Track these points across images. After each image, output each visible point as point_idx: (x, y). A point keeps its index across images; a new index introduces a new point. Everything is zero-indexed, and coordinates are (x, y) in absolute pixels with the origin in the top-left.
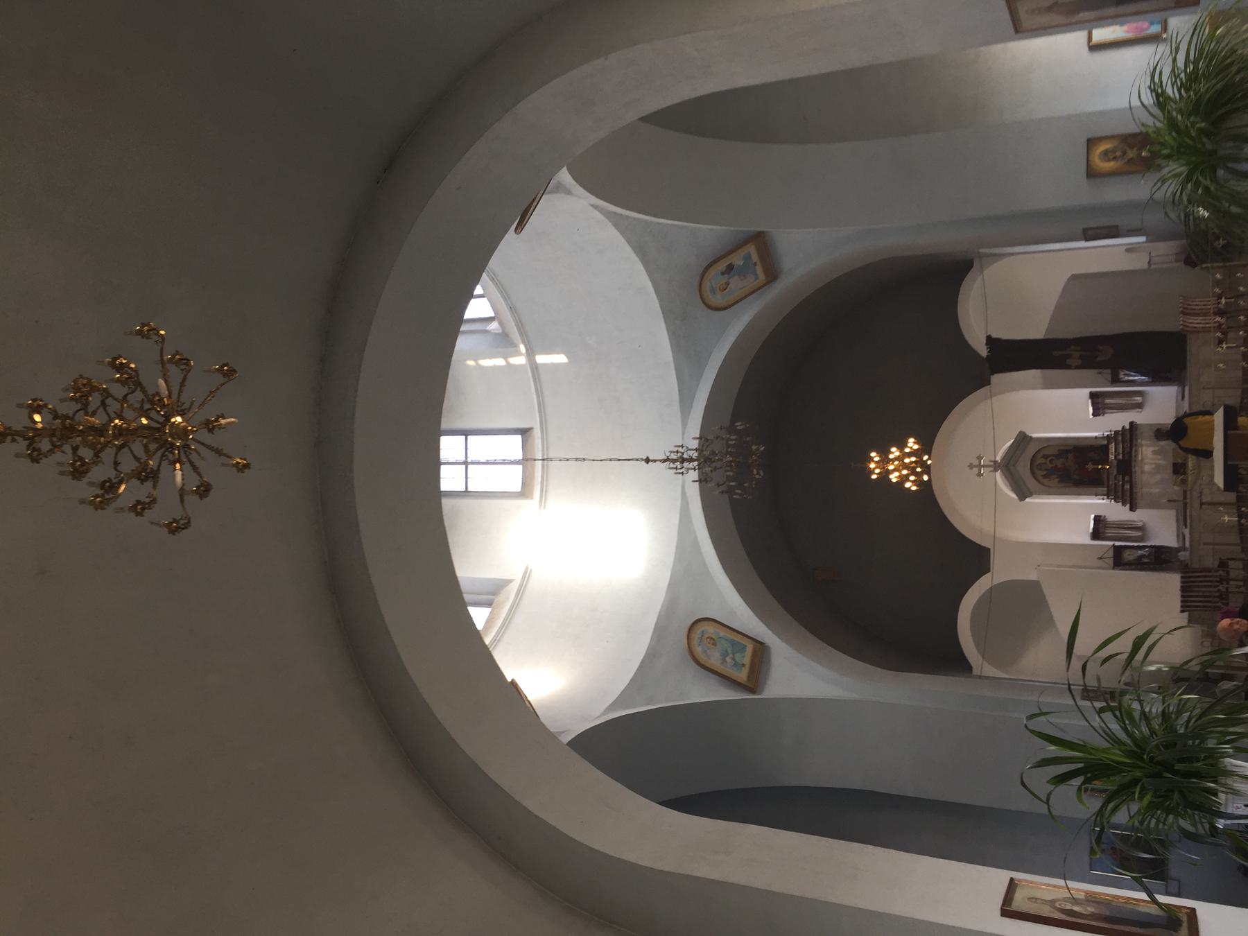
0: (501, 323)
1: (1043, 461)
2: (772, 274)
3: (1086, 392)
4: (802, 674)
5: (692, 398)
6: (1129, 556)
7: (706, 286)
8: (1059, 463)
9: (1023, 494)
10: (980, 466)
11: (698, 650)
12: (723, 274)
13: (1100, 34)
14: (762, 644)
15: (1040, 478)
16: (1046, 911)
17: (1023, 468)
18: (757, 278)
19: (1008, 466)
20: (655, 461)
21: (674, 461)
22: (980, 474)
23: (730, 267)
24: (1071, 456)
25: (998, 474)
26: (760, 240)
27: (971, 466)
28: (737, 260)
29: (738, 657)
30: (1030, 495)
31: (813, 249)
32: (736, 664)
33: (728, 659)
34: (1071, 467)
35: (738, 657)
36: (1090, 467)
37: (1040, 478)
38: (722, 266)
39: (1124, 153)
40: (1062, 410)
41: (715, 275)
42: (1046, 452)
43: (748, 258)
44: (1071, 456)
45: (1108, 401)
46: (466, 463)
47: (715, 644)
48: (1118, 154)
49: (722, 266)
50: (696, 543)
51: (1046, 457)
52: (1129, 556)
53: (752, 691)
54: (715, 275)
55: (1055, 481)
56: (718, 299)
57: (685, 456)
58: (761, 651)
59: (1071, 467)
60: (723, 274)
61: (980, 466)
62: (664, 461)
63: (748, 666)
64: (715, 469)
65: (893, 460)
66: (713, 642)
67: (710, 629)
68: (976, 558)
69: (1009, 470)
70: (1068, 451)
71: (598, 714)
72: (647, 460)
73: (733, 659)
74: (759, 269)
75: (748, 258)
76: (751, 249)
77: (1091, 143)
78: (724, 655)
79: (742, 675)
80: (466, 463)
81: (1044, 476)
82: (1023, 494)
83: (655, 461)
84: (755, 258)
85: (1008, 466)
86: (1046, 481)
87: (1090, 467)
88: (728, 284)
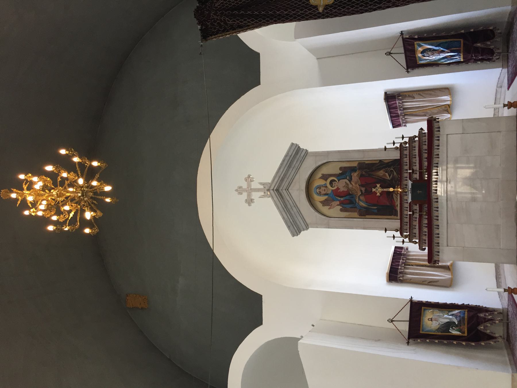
0: (419, 139)
1: (322, 182)
3: (379, 88)
6: (432, 322)
8: (341, 185)
9: (296, 227)
13: (445, 244)
16: (443, 90)
19: (279, 190)
24: (355, 175)
27: (240, 190)
36: (378, 190)
37: (320, 206)
42: (325, 171)
44: (355, 175)
45: (407, 105)
51: (325, 177)
52: (432, 322)
55: (336, 210)
61: (250, 190)
65: (41, 210)
68: (247, 309)
69: (281, 195)
70: (353, 169)
81: (325, 203)
82: (296, 227)
85: (279, 190)
86: (325, 209)
87: (378, 190)
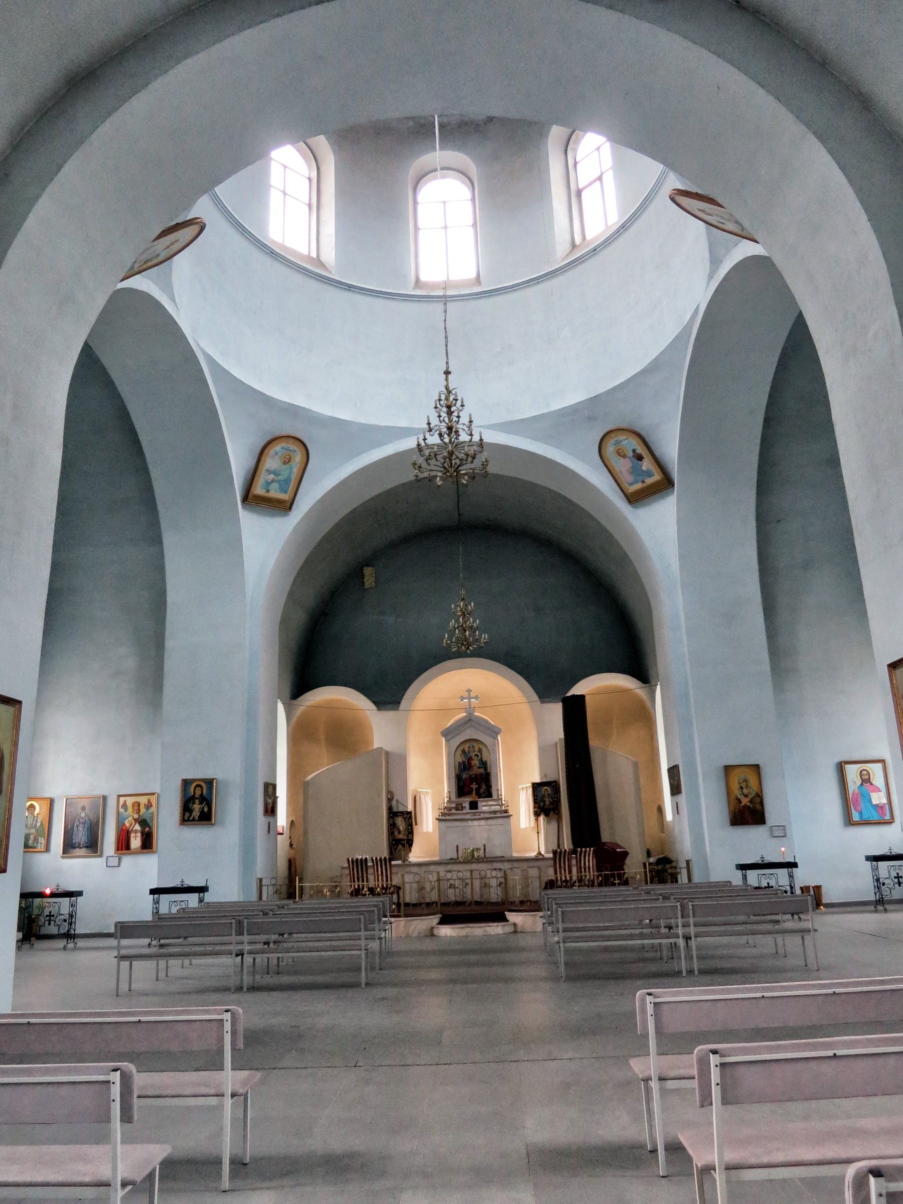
1: (476, 749)
2: (635, 499)
4: (266, 549)
5: (517, 433)
7: (622, 437)
8: (476, 762)
9: (448, 734)
10: (469, 698)
11: (278, 448)
12: (634, 451)
14: (290, 508)
15: (461, 748)
17: (469, 734)
18: (631, 484)
20: (447, 380)
21: (447, 399)
22: (462, 698)
23: (640, 458)
24: (482, 771)
25: (465, 714)
26: (666, 483)
28: (647, 464)
29: (275, 486)
30: (447, 741)
31: (657, 534)
32: (268, 484)
33: (272, 476)
34: (473, 781)
35: (275, 486)
36: (474, 786)
38: (641, 450)
39: (746, 796)
40: (524, 762)
41: (631, 444)
43: (649, 474)
44: (482, 771)
46: (446, 227)
47: (285, 463)
48: (745, 791)
49: (641, 450)
50: (381, 444)
51: (480, 751)
53: (245, 499)
54: (631, 444)
55: (460, 759)
56: (610, 449)
57: (453, 409)
58: (284, 507)
59: (473, 781)
60: (634, 451)
61: (469, 698)
62: (447, 388)
63: (267, 495)
64: (441, 435)
66: (287, 461)
67: (298, 458)
70: (486, 769)
71: (202, 345)
72: (447, 373)
73: (273, 481)
74: (638, 486)
75: (649, 474)
76: (657, 477)
77: (756, 768)
78: (275, 473)
79: (259, 490)
80: (446, 227)
81: (463, 751)
82: (448, 734)
83: (447, 380)
84: (649, 481)
86: (459, 752)
87: (474, 786)
88: (624, 456)
